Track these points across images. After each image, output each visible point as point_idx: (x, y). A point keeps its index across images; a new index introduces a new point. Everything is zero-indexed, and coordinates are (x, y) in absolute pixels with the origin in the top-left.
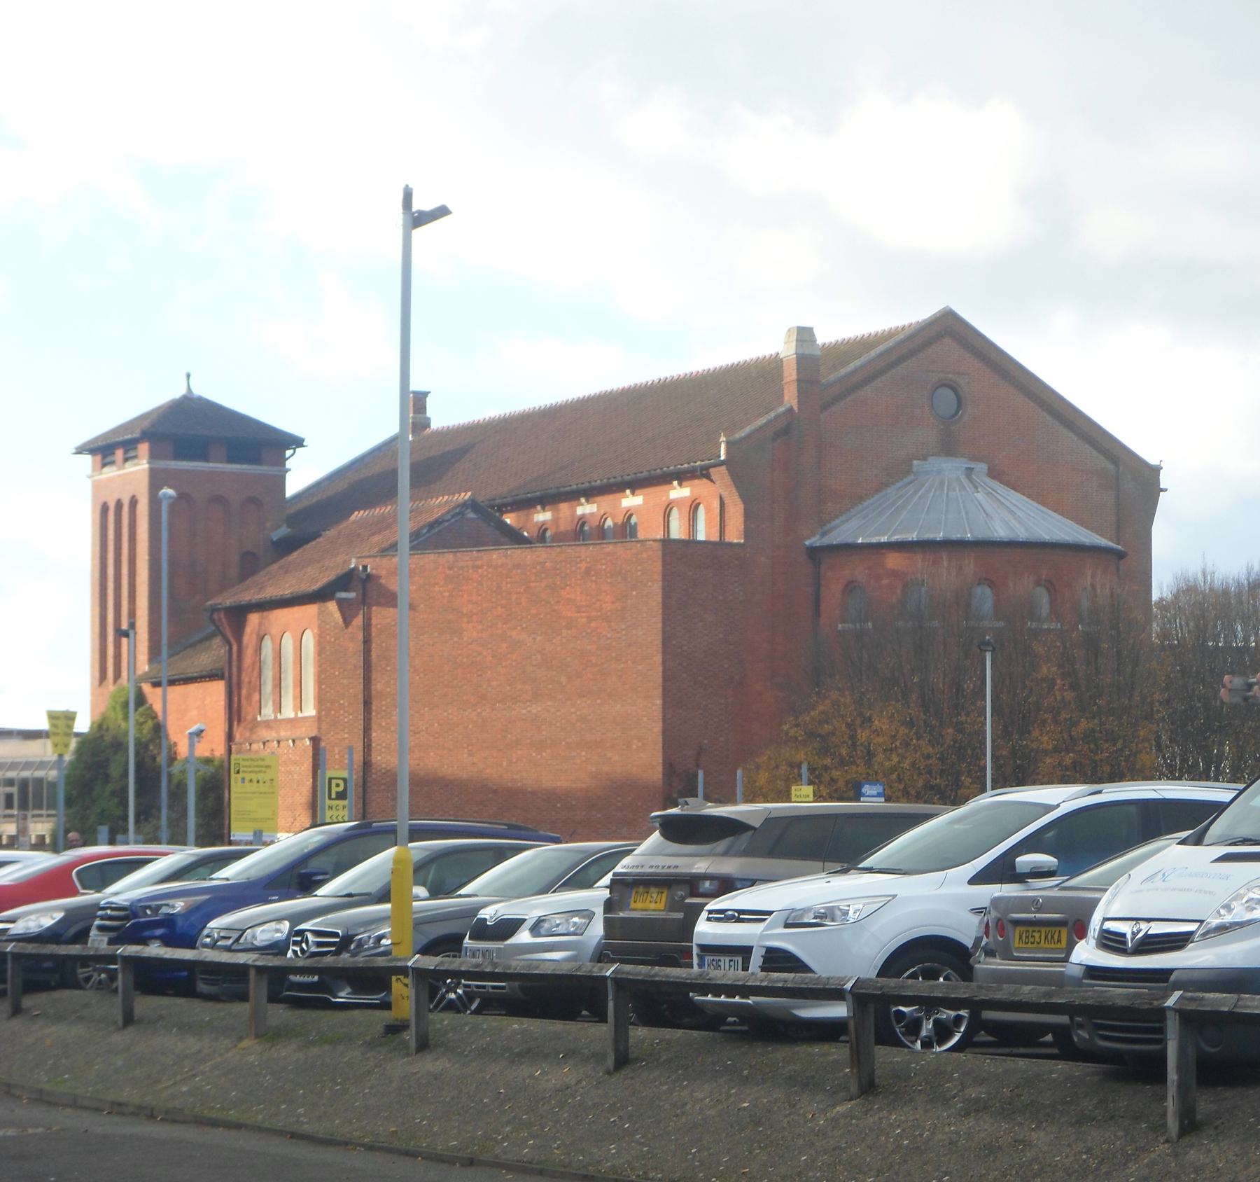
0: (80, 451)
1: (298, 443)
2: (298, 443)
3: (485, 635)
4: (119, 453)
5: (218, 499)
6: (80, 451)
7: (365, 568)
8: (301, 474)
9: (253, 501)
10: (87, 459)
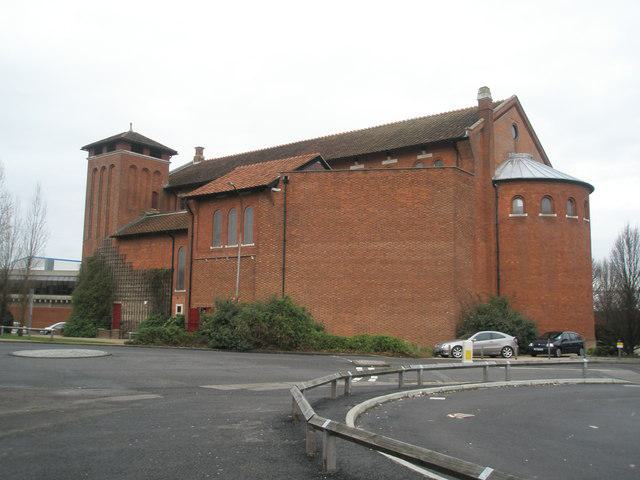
0: (83, 149)
1: (175, 153)
2: (175, 153)
3: (354, 210)
4: (105, 150)
5: (145, 170)
6: (83, 149)
7: (286, 177)
8: (175, 164)
9: (157, 172)
10: (86, 153)
